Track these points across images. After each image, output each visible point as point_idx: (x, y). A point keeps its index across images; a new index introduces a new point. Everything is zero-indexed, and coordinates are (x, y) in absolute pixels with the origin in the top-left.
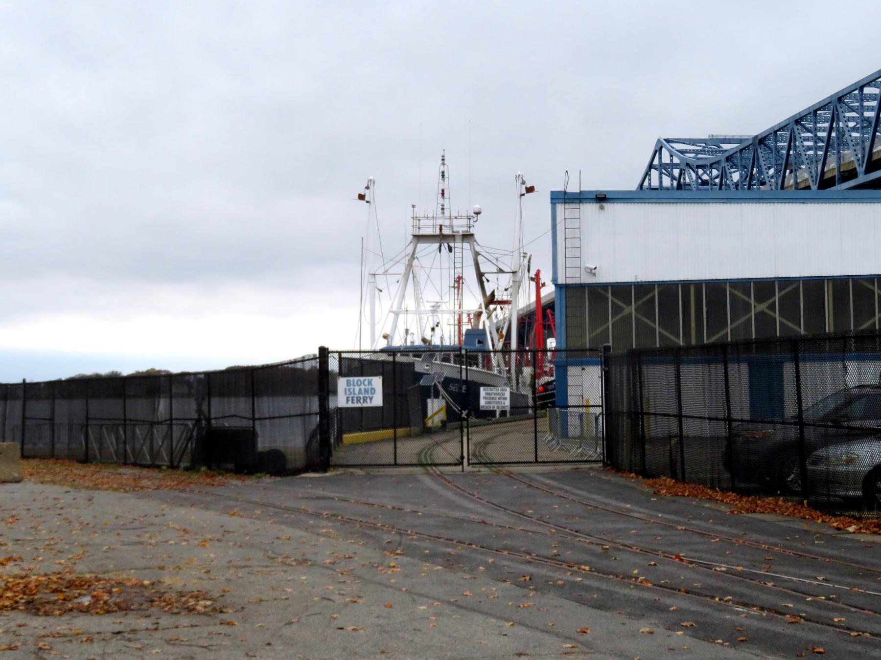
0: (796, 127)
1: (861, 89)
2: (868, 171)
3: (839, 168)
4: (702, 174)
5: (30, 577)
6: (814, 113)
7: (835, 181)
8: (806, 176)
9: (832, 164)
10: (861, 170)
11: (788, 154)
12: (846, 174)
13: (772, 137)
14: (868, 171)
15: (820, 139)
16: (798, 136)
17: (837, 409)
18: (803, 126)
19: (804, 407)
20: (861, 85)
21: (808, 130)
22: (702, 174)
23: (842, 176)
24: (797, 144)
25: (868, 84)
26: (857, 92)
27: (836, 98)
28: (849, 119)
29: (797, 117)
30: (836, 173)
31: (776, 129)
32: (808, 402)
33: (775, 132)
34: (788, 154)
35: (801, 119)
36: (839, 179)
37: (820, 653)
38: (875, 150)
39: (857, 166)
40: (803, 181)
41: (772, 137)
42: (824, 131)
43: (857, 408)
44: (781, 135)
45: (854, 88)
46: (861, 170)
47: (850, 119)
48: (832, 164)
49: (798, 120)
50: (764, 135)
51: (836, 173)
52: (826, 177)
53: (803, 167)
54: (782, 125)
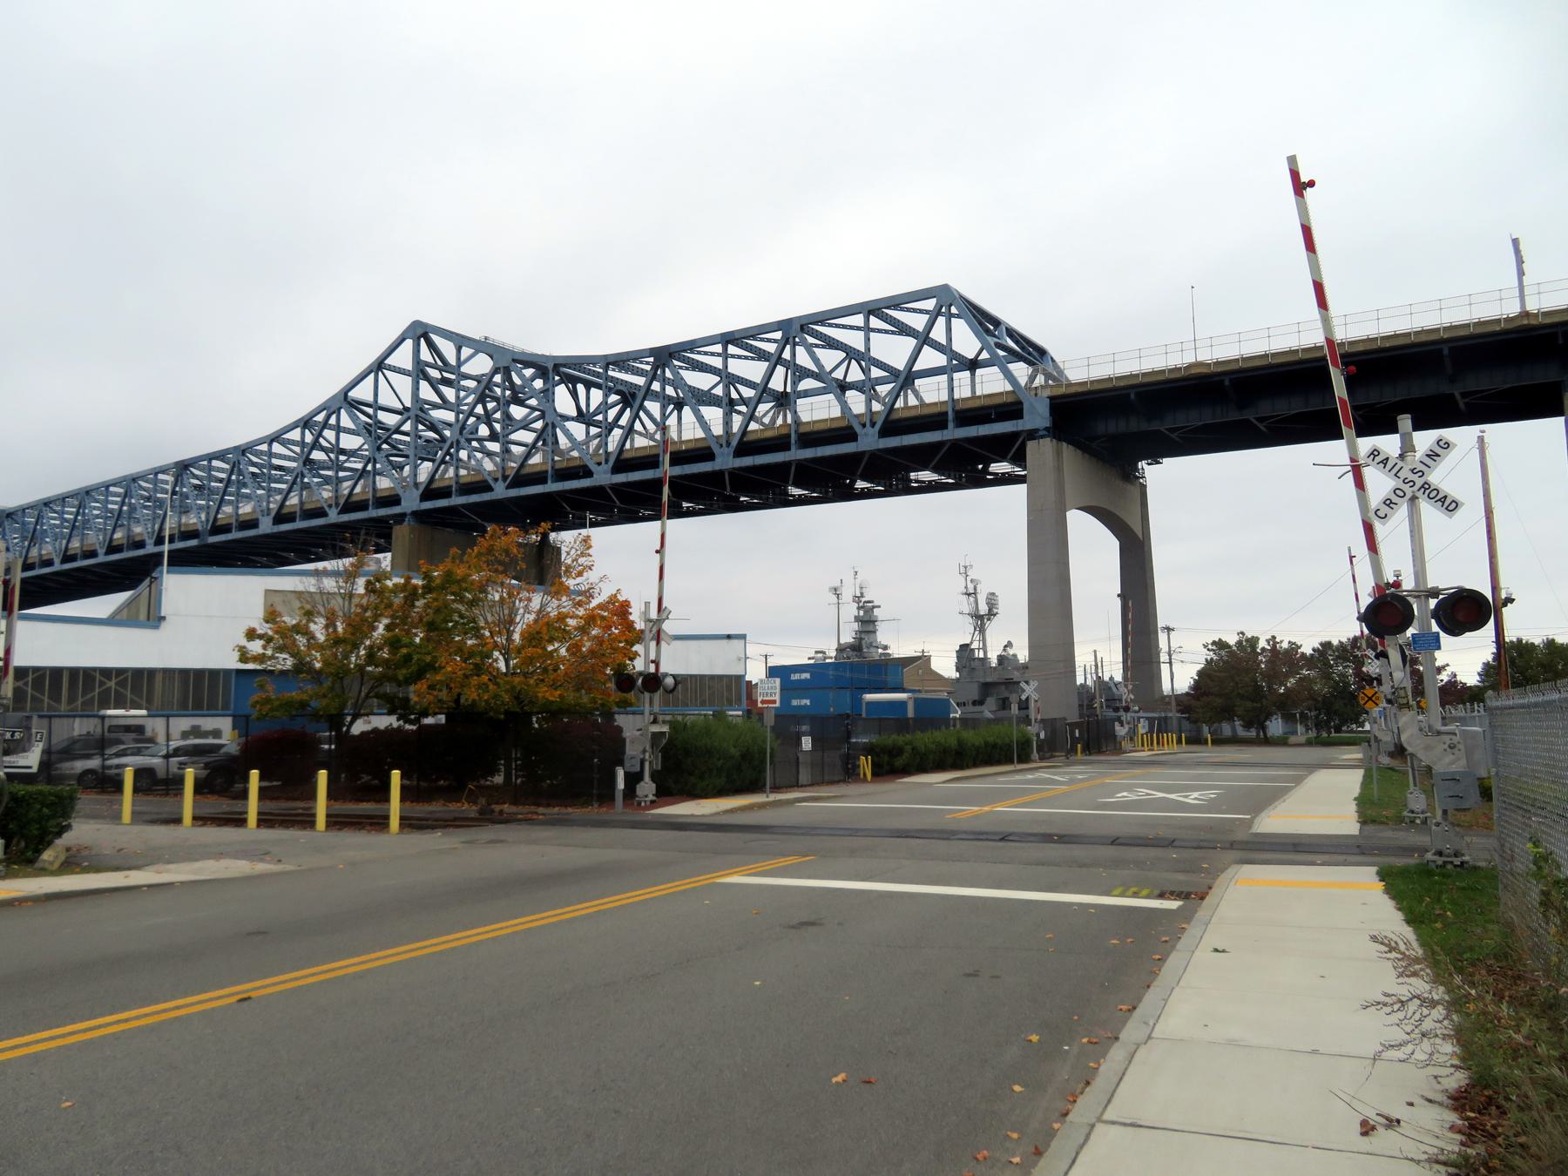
0: (44, 509)
1: (156, 474)
2: (108, 552)
3: (82, 548)
4: (769, 375)
5: (1484, 1156)
6: (63, 499)
7: (232, 528)
8: (50, 548)
9: (294, 500)
10: (101, 551)
11: (35, 530)
12: (87, 553)
13: (19, 513)
14: (108, 552)
15: (67, 520)
16: (45, 516)
17: (69, 746)
18: (51, 508)
19: (52, 743)
20: (107, 484)
21: (55, 512)
22: (769, 375)
23: (239, 525)
24: (87, 511)
25: (114, 485)
26: (151, 476)
27: (84, 490)
28: (95, 508)
29: (46, 501)
30: (79, 551)
31: (25, 507)
32: (54, 741)
33: (24, 510)
34: (35, 530)
35: (50, 502)
36: (39, 565)
37: (1166, 941)
38: (288, 503)
39: (147, 538)
40: (47, 554)
41: (19, 513)
42: (71, 514)
43: (77, 746)
44: (68, 501)
45: (150, 472)
46: (101, 551)
47: (94, 508)
48: (34, 552)
49: (47, 503)
50: (11, 511)
51: (37, 560)
52: (285, 511)
53: (48, 540)
54: (32, 505)
